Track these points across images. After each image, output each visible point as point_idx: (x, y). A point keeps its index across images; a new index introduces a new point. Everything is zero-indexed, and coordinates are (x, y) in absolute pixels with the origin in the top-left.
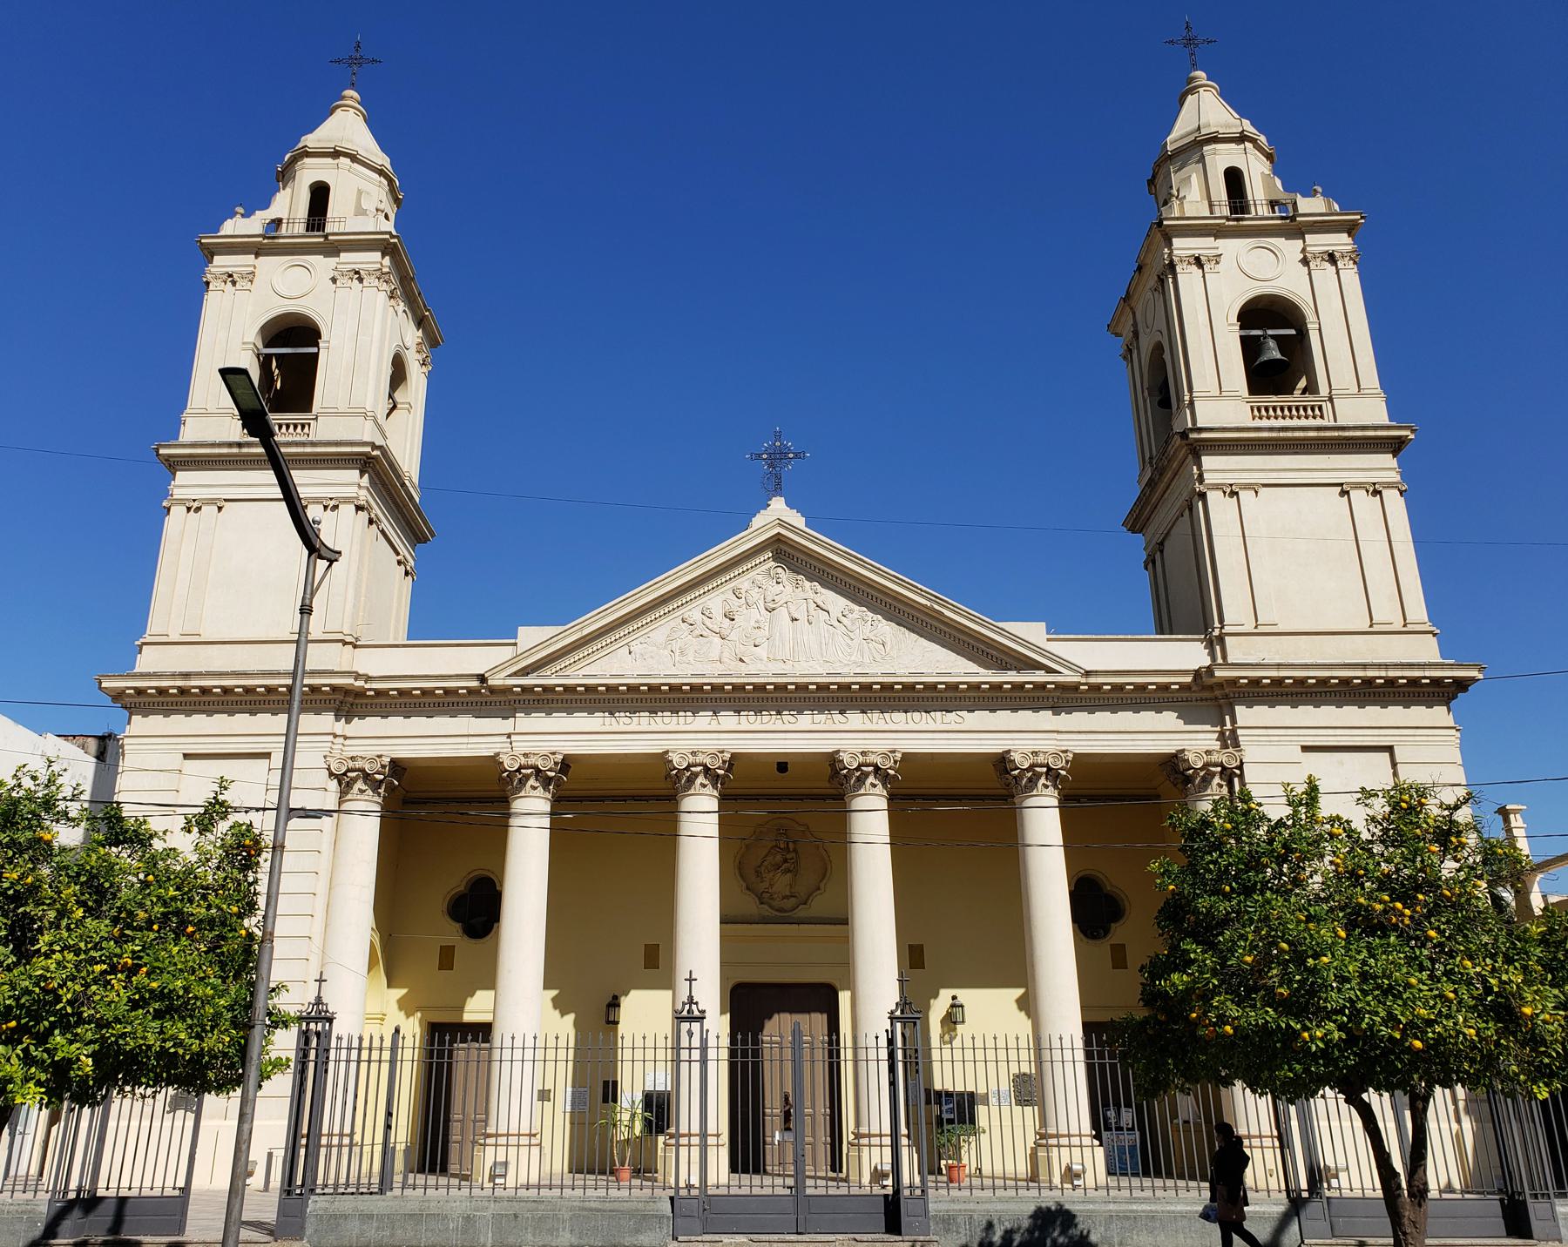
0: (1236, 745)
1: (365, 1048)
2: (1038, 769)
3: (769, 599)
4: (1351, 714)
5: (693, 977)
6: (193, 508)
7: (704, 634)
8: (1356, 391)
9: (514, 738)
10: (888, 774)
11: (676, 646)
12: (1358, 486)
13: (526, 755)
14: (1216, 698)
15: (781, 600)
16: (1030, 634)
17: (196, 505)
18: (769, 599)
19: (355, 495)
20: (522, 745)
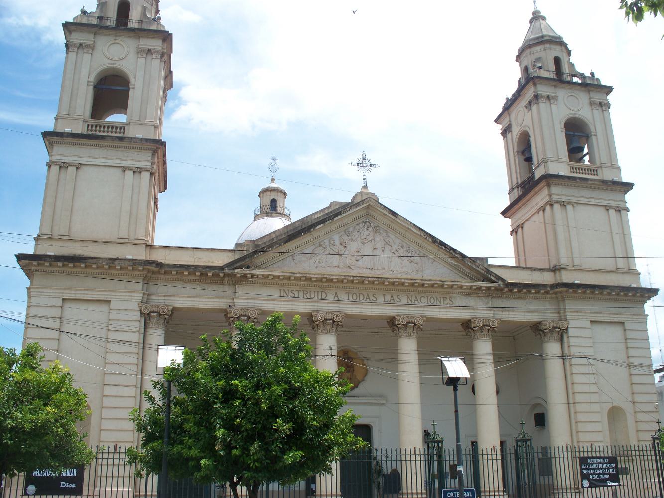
1: (115, 477)
3: (363, 237)
12: (612, 208)
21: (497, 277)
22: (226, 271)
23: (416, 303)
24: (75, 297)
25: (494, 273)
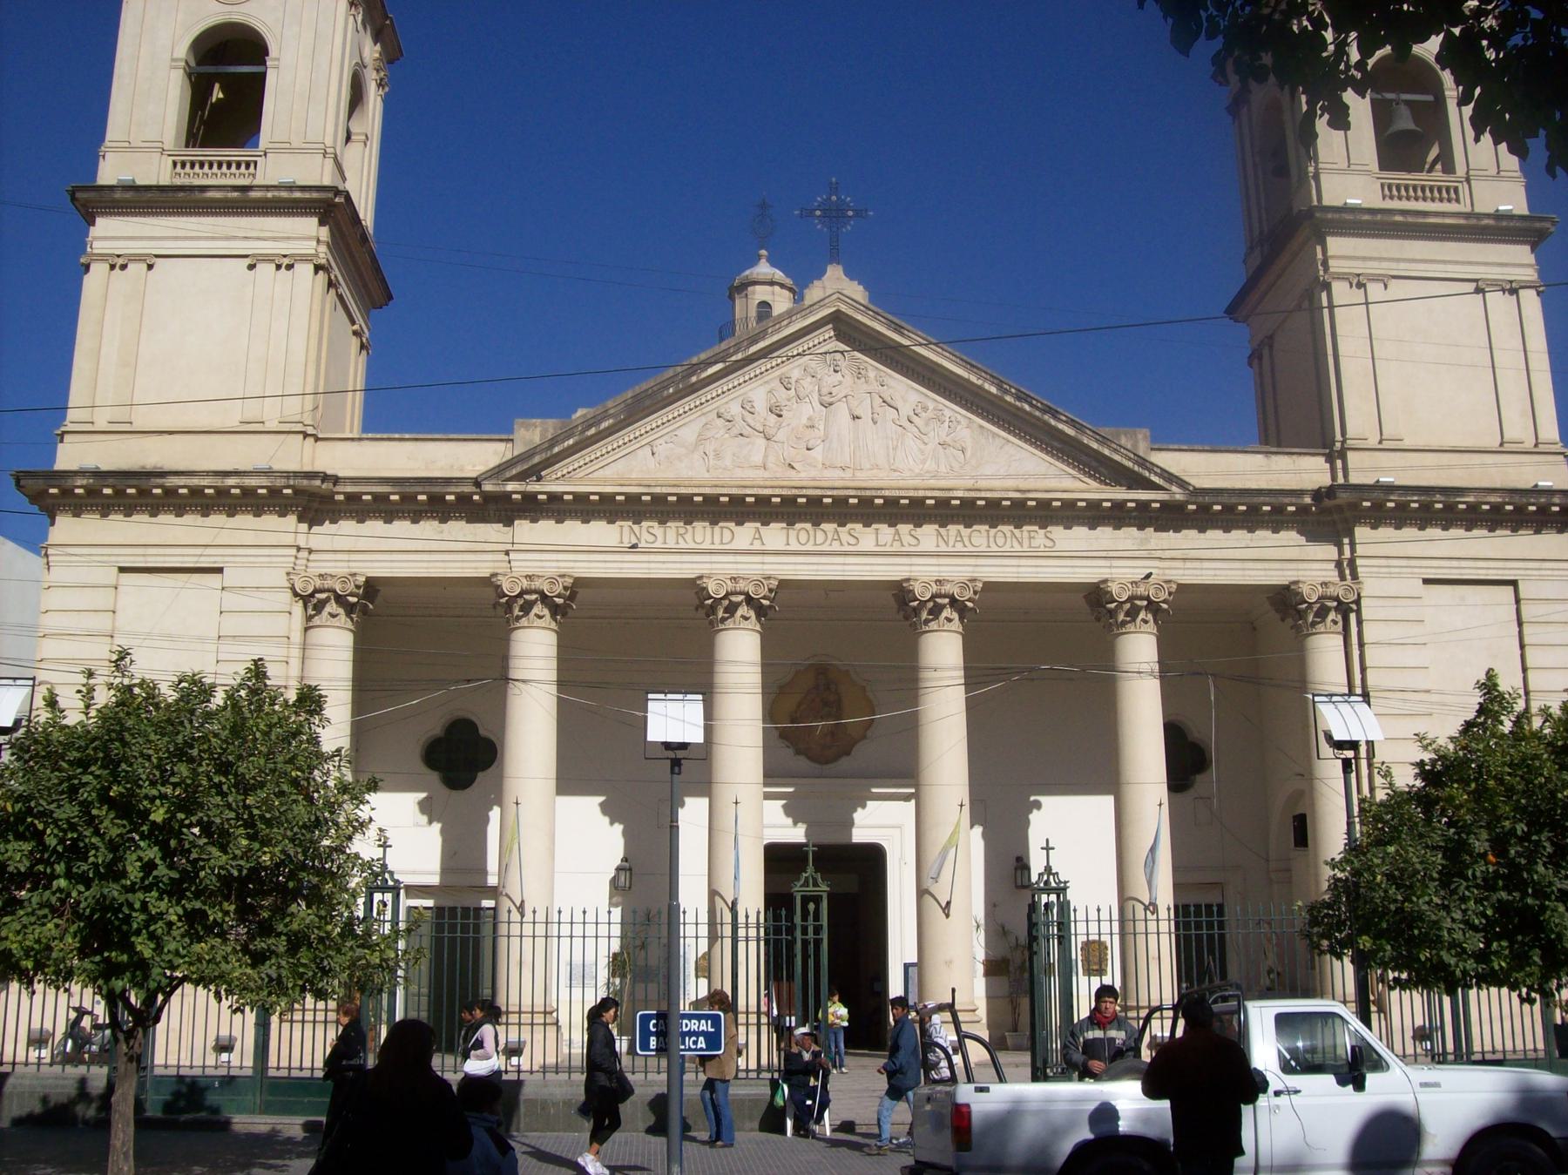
0: (1355, 576)
2: (1138, 603)
3: (825, 391)
4: (305, 243)
5: (1051, 845)
6: (118, 264)
7: (745, 433)
8: (1494, 171)
9: (512, 556)
10: (966, 606)
11: (710, 448)
13: (529, 577)
14: (1334, 522)
15: (840, 392)
16: (1131, 445)
17: (120, 261)
18: (825, 391)
19: (313, 252)
20: (524, 564)
21: (1166, 475)
22: (488, 487)
23: (959, 547)
24: (146, 562)
25: (1158, 467)
